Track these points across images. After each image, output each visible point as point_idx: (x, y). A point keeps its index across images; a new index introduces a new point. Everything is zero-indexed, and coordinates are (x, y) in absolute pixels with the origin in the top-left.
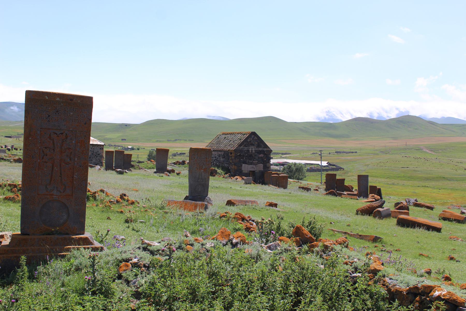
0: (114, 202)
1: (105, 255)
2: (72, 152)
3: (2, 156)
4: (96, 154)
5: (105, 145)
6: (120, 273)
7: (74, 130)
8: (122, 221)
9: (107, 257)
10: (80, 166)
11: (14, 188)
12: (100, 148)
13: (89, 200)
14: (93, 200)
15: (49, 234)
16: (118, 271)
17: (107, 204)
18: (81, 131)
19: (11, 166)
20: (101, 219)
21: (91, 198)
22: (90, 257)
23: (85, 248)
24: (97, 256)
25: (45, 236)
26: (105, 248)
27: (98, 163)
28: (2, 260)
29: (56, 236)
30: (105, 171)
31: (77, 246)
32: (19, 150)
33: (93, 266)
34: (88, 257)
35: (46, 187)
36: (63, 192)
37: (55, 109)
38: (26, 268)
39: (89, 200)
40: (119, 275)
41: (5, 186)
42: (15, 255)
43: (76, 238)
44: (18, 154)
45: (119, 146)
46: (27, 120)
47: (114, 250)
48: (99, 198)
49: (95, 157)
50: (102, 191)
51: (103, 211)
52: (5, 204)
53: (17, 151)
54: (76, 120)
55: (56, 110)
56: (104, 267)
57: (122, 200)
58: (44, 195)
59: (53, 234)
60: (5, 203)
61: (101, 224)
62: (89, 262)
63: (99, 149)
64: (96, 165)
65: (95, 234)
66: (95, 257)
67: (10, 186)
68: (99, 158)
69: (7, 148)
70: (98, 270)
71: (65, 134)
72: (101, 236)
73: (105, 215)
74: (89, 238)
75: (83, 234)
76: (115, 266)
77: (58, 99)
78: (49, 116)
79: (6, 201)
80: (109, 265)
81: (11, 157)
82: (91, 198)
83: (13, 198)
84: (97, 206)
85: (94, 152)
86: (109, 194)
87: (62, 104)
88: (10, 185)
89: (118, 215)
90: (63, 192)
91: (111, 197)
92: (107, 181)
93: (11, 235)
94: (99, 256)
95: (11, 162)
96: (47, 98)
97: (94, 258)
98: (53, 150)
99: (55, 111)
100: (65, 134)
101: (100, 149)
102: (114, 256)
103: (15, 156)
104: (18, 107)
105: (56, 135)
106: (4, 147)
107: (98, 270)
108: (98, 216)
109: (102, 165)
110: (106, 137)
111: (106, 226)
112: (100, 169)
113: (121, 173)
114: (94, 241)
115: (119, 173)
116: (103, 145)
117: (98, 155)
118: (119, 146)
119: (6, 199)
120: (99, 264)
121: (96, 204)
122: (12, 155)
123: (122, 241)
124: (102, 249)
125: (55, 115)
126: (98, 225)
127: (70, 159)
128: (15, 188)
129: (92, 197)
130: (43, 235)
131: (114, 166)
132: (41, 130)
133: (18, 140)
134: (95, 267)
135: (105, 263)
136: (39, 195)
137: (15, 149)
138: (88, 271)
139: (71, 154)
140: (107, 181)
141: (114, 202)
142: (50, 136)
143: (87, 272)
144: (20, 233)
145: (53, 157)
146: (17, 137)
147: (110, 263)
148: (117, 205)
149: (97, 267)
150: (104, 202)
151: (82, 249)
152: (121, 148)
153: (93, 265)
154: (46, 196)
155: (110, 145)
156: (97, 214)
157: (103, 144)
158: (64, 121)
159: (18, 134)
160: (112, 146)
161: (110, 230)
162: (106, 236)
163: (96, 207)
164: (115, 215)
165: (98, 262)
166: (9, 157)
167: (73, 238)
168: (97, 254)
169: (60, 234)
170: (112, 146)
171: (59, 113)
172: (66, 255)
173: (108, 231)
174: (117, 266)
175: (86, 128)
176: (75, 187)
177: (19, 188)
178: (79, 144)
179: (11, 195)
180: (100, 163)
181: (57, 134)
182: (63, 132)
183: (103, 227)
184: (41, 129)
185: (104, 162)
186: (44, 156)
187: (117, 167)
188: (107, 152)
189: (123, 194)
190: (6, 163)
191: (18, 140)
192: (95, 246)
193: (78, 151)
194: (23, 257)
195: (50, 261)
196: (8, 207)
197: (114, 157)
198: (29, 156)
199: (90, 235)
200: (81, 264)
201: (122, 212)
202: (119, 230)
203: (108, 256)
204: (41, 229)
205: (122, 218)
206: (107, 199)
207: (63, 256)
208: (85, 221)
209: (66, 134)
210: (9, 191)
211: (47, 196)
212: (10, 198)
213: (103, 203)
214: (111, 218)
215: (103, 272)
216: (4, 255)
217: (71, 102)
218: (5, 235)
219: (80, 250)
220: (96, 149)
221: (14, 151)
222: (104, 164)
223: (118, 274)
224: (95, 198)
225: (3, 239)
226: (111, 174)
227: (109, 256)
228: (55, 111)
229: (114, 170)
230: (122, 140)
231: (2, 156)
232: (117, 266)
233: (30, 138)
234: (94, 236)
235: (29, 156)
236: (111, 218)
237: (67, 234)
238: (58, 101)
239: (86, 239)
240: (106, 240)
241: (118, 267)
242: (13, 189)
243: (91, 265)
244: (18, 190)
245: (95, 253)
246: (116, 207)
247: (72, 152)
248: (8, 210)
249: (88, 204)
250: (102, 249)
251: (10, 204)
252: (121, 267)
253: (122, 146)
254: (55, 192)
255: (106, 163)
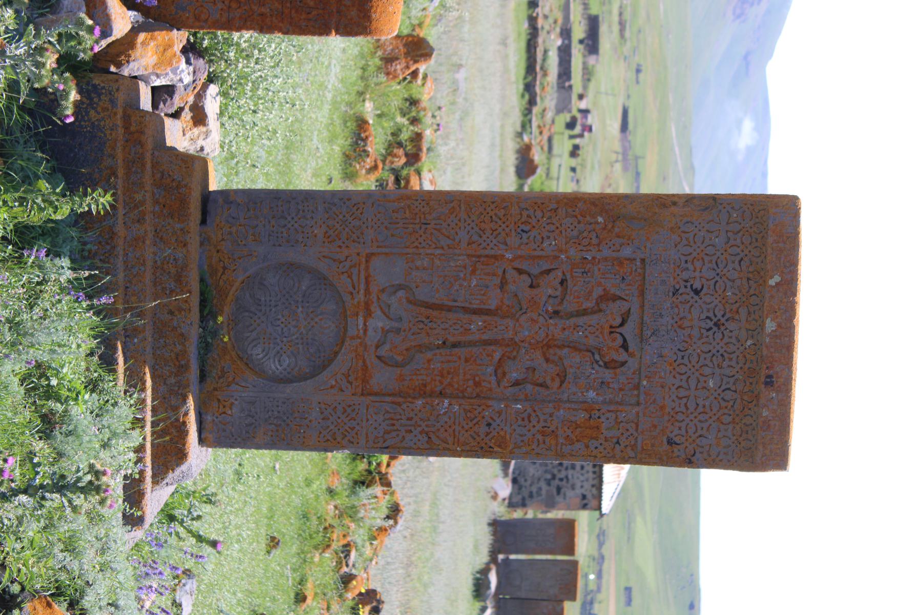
0: (347, 566)
1: (107, 536)
2: (547, 387)
3: (542, 99)
4: (561, 480)
5: (602, 515)
6: (22, 601)
7: (642, 398)
8: (258, 601)
9: (98, 545)
10: (489, 425)
11: (406, 155)
12: (589, 496)
13: (354, 459)
14: (355, 476)
15: (203, 303)
16: (35, 594)
17: (335, 536)
18: (637, 426)
19: (502, 135)
20: (270, 509)
21: (362, 466)
22: (98, 474)
23: (140, 449)
24: (102, 502)
25: (195, 286)
26: (138, 534)
27: (520, 488)
28: (102, 123)
29: (194, 332)
30: (485, 520)
31: (149, 418)
32: (573, 162)
33: (61, 485)
34: (98, 467)
35: (400, 287)
36: (379, 358)
37: (728, 315)
38: (63, 212)
39: (354, 459)
40: (14, 597)
41: (414, 121)
42: (121, 172)
43: (186, 414)
44: (555, 162)
45: (599, 575)
46: (675, 204)
47: (126, 572)
48: (365, 501)
49: (549, 476)
50: (394, 512)
51: (305, 516)
52: (338, 122)
53: (566, 155)
54: (685, 400)
55: (723, 320)
56: (52, 535)
57: (354, 599)
58: (367, 278)
59: (203, 318)
60: (345, 122)
61: (249, 510)
62: (78, 471)
63: (583, 491)
64: (515, 481)
65: (204, 490)
66: (98, 493)
67: (412, 140)
68: (544, 492)
69: (578, 116)
70: (42, 506)
71: (623, 356)
72: (195, 514)
73: (287, 529)
74: (184, 467)
75: (202, 441)
76: (57, 581)
77: (770, 326)
78: (697, 292)
79: (352, 125)
80: (61, 556)
81: (541, 133)
82: (362, 466)
83: (365, 151)
84: (331, 492)
85: (570, 472)
86: (382, 542)
87: (749, 342)
88: (417, 138)
89: (290, 582)
90: (379, 358)
91: (368, 551)
92: (441, 526)
93: (205, 152)
94: (105, 511)
95: (520, 135)
96: (772, 282)
97: (93, 488)
98: (556, 313)
99: (719, 315)
100: (623, 356)
101: (584, 497)
102: (100, 575)
103: (546, 148)
104: (750, 150)
105: (619, 320)
106: (583, 105)
107: (42, 506)
108: (283, 498)
109: (512, 504)
110: (639, 520)
111: (239, 535)
112: (495, 497)
113: (479, 588)
114: (171, 489)
115: (477, 579)
116: (599, 508)
117: (559, 490)
118: (599, 575)
119: (362, 124)
120: (68, 510)
121: (336, 485)
122: (550, 140)
123: (169, 603)
124: (133, 521)
125: (703, 316)
126: (243, 498)
127: (517, 383)
128: (403, 160)
129: (369, 472)
130: (202, 280)
131: (513, 557)
132: (635, 259)
133: (614, 157)
134: (55, 495)
135: (70, 538)
136: (367, 261)
137: (576, 147)
138: (39, 464)
139: (541, 385)
140: (441, 526)
141: (347, 566)
142: (615, 298)
143: (36, 460)
144: (213, 186)
145: (525, 313)
146: (625, 154)
147: (68, 559)
148: (331, 579)
149: (56, 505)
150: (347, 521)
151: (136, 438)
152: (592, 586)
153: (63, 487)
154: (362, 286)
155: (601, 537)
156: (295, 493)
157: (606, 506)
158: (680, 354)
159: (637, 158)
160: (601, 545)
161: (219, 552)
162: (194, 536)
163: (324, 487)
164: (288, 572)
165: (75, 509)
166: (539, 127)
167: (184, 399)
168: (109, 502)
169: (205, 347)
170: (601, 545)
171: (711, 333)
172: (114, 371)
173: (214, 544)
174: (57, 588)
175: (653, 445)
176: (399, 404)
177: (404, 173)
178: (583, 415)
179: (376, 144)
180: (523, 499)
181: (622, 325)
182: (630, 350)
183: (233, 523)
184: (643, 261)
185: (530, 515)
186: (529, 275)
187: (505, 570)
188: (568, 528)
189: (380, 602)
190: (516, 118)
191: (614, 157)
192: (149, 490)
193: (551, 415)
194: (106, 200)
195: (90, 307)
196: (325, 134)
197: (550, 557)
198: (529, 216)
199: (195, 471)
200: (69, 433)
201: (300, 598)
202: (220, 590)
203: (103, 551)
204: (225, 268)
205: (274, 600)
206: (358, 535)
207: (108, 362)
208: (258, 447)
209: (623, 364)
210: (393, 134)
211: (362, 292)
212: (365, 140)
213: (340, 516)
214: (274, 551)
215: (32, 529)
216: (121, 131)
217: (763, 379)
218: (203, 129)
219: (133, 429)
220: (582, 478)
221: (568, 145)
222: (518, 514)
223: (17, 596)
224: (363, 483)
225: (191, 123)
226: (476, 547)
227: (103, 553)
228: (719, 315)
229: (493, 559)
230: (628, 590)
231: (542, 99)
232: (57, 588)
233: (600, 219)
234: (195, 484)
235: (529, 216)
236: (276, 552)
237: (203, 377)
238: (762, 326)
239: (181, 456)
240: (177, 534)
241: (52, 595)
242: (401, 152)
243: (63, 477)
244: (397, 173)
245: (120, 491)
246: (325, 574)
247: (547, 387)
248: (316, 133)
249: (337, 459)
250: (133, 521)
251: (341, 141)
252: (49, 605)
253: (599, 590)
254: (380, 324)
255: (523, 522)
